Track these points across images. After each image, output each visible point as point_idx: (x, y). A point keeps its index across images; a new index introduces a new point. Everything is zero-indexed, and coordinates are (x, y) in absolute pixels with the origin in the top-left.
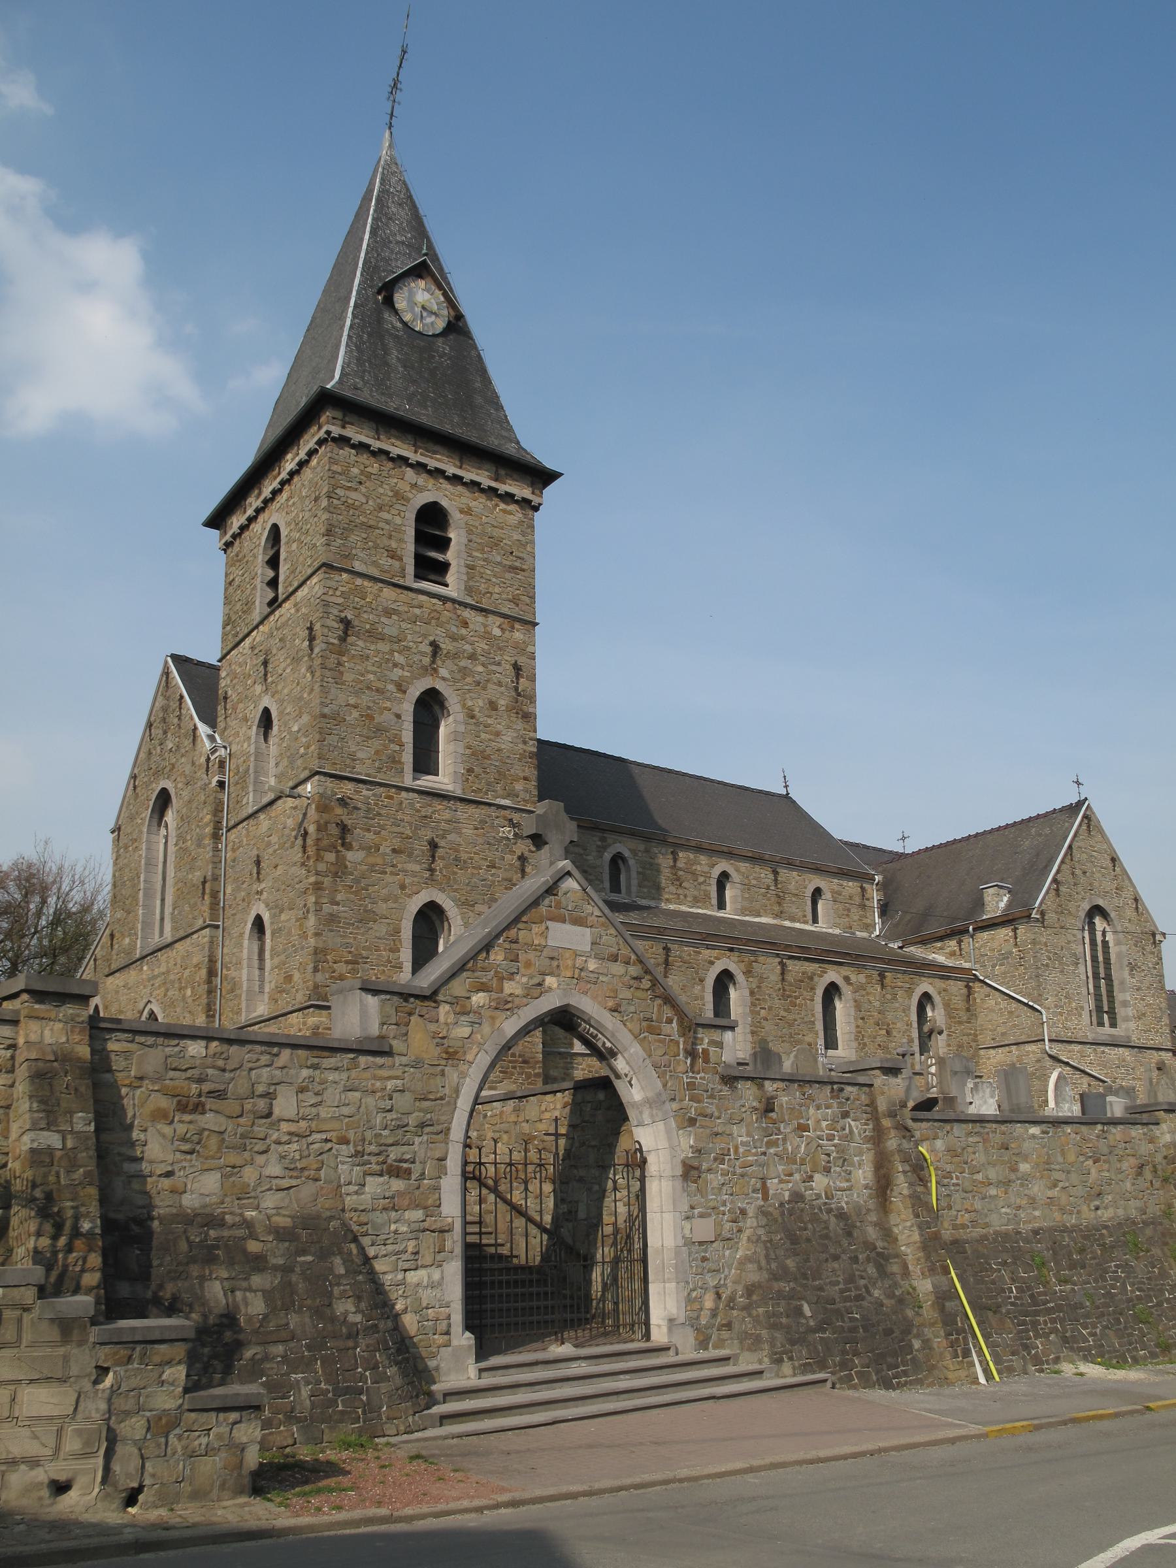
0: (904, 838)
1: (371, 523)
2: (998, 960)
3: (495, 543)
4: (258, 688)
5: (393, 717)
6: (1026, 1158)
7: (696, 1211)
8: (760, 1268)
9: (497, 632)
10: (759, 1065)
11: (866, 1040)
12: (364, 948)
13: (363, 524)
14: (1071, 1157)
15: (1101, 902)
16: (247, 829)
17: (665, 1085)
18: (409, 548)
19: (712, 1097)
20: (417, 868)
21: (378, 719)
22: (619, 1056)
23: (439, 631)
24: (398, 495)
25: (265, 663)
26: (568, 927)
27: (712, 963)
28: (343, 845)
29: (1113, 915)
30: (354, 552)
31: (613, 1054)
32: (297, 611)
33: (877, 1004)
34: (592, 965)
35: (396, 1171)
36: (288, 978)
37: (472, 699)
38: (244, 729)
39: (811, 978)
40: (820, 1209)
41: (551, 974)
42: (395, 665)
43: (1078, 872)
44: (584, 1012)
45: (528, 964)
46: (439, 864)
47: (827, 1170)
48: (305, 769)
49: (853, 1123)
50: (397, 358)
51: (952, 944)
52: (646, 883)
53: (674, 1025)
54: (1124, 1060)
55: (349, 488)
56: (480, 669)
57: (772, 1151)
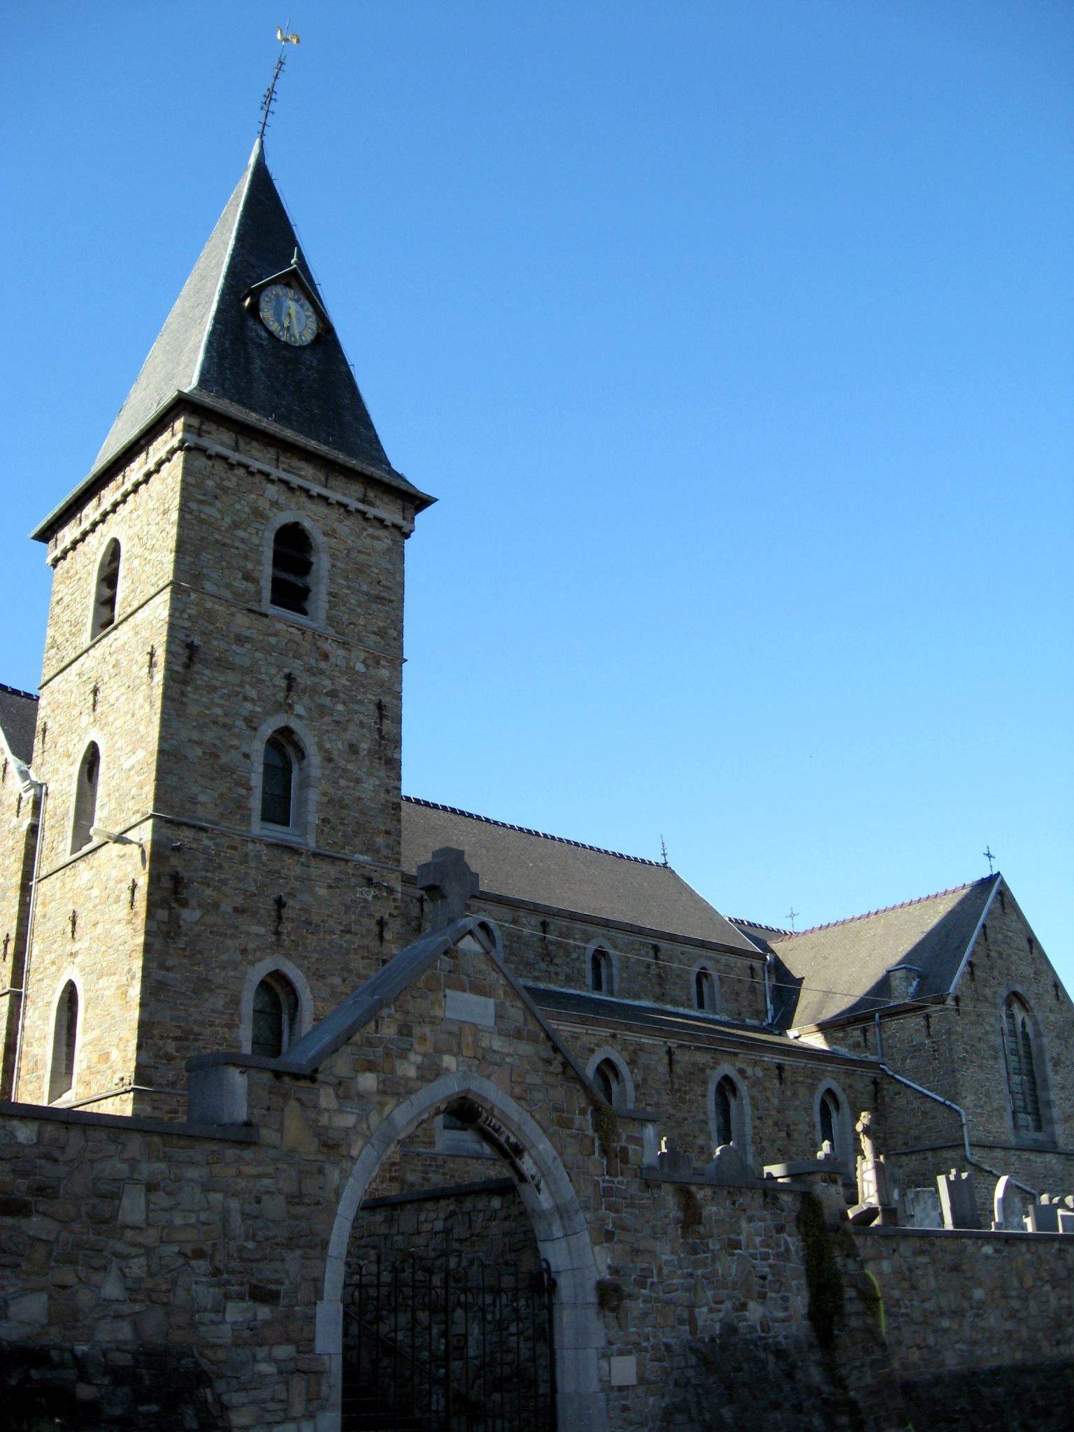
0: (792, 916)
1: (226, 541)
2: (909, 1052)
3: (361, 569)
4: (86, 719)
5: (240, 756)
6: (979, 1284)
7: (615, 1348)
8: (691, 1420)
9: (360, 667)
10: (666, 1169)
11: (765, 1143)
12: (196, 1022)
13: (217, 541)
14: (1029, 1282)
15: (1018, 988)
16: (62, 880)
17: (578, 1192)
18: (266, 571)
19: (632, 1205)
20: (262, 930)
21: (224, 759)
22: (526, 1154)
23: (298, 663)
24: (257, 513)
25: (95, 691)
26: (468, 996)
27: (592, 1051)
28: (177, 900)
29: (1032, 1003)
30: (205, 571)
31: (518, 1150)
32: (137, 633)
33: (775, 1101)
34: (497, 1044)
35: (262, 1295)
36: (105, 1057)
37: (331, 741)
38: (65, 765)
39: (702, 1070)
40: (756, 1346)
41: (450, 1052)
42: (246, 699)
43: (993, 954)
44: (485, 1099)
45: (423, 1039)
46: (287, 927)
47: (762, 1296)
48: (138, 811)
49: (789, 1239)
50: (262, 369)
51: (856, 1034)
52: (513, 958)
53: (589, 1117)
54: (1052, 1169)
55: (202, 502)
56: (340, 707)
57: (699, 1272)
